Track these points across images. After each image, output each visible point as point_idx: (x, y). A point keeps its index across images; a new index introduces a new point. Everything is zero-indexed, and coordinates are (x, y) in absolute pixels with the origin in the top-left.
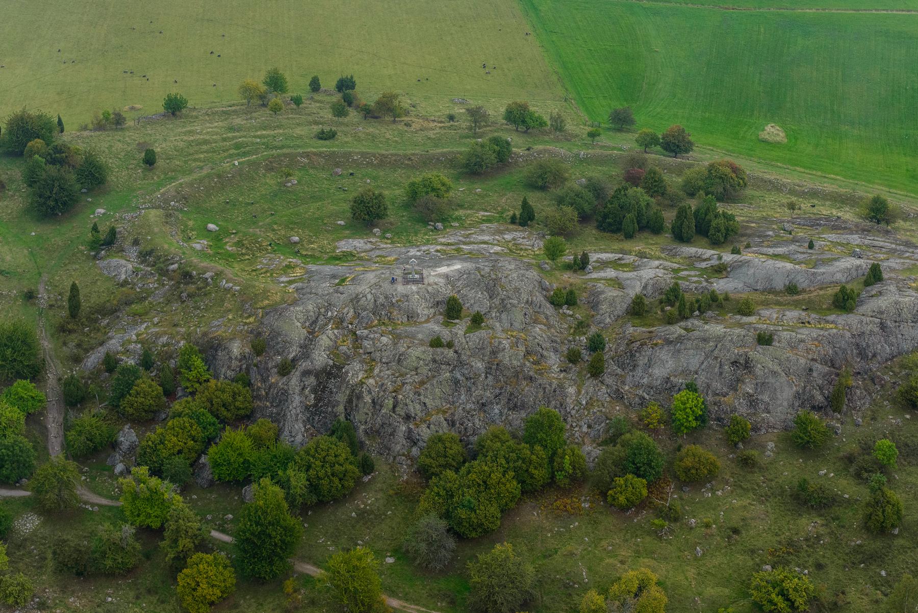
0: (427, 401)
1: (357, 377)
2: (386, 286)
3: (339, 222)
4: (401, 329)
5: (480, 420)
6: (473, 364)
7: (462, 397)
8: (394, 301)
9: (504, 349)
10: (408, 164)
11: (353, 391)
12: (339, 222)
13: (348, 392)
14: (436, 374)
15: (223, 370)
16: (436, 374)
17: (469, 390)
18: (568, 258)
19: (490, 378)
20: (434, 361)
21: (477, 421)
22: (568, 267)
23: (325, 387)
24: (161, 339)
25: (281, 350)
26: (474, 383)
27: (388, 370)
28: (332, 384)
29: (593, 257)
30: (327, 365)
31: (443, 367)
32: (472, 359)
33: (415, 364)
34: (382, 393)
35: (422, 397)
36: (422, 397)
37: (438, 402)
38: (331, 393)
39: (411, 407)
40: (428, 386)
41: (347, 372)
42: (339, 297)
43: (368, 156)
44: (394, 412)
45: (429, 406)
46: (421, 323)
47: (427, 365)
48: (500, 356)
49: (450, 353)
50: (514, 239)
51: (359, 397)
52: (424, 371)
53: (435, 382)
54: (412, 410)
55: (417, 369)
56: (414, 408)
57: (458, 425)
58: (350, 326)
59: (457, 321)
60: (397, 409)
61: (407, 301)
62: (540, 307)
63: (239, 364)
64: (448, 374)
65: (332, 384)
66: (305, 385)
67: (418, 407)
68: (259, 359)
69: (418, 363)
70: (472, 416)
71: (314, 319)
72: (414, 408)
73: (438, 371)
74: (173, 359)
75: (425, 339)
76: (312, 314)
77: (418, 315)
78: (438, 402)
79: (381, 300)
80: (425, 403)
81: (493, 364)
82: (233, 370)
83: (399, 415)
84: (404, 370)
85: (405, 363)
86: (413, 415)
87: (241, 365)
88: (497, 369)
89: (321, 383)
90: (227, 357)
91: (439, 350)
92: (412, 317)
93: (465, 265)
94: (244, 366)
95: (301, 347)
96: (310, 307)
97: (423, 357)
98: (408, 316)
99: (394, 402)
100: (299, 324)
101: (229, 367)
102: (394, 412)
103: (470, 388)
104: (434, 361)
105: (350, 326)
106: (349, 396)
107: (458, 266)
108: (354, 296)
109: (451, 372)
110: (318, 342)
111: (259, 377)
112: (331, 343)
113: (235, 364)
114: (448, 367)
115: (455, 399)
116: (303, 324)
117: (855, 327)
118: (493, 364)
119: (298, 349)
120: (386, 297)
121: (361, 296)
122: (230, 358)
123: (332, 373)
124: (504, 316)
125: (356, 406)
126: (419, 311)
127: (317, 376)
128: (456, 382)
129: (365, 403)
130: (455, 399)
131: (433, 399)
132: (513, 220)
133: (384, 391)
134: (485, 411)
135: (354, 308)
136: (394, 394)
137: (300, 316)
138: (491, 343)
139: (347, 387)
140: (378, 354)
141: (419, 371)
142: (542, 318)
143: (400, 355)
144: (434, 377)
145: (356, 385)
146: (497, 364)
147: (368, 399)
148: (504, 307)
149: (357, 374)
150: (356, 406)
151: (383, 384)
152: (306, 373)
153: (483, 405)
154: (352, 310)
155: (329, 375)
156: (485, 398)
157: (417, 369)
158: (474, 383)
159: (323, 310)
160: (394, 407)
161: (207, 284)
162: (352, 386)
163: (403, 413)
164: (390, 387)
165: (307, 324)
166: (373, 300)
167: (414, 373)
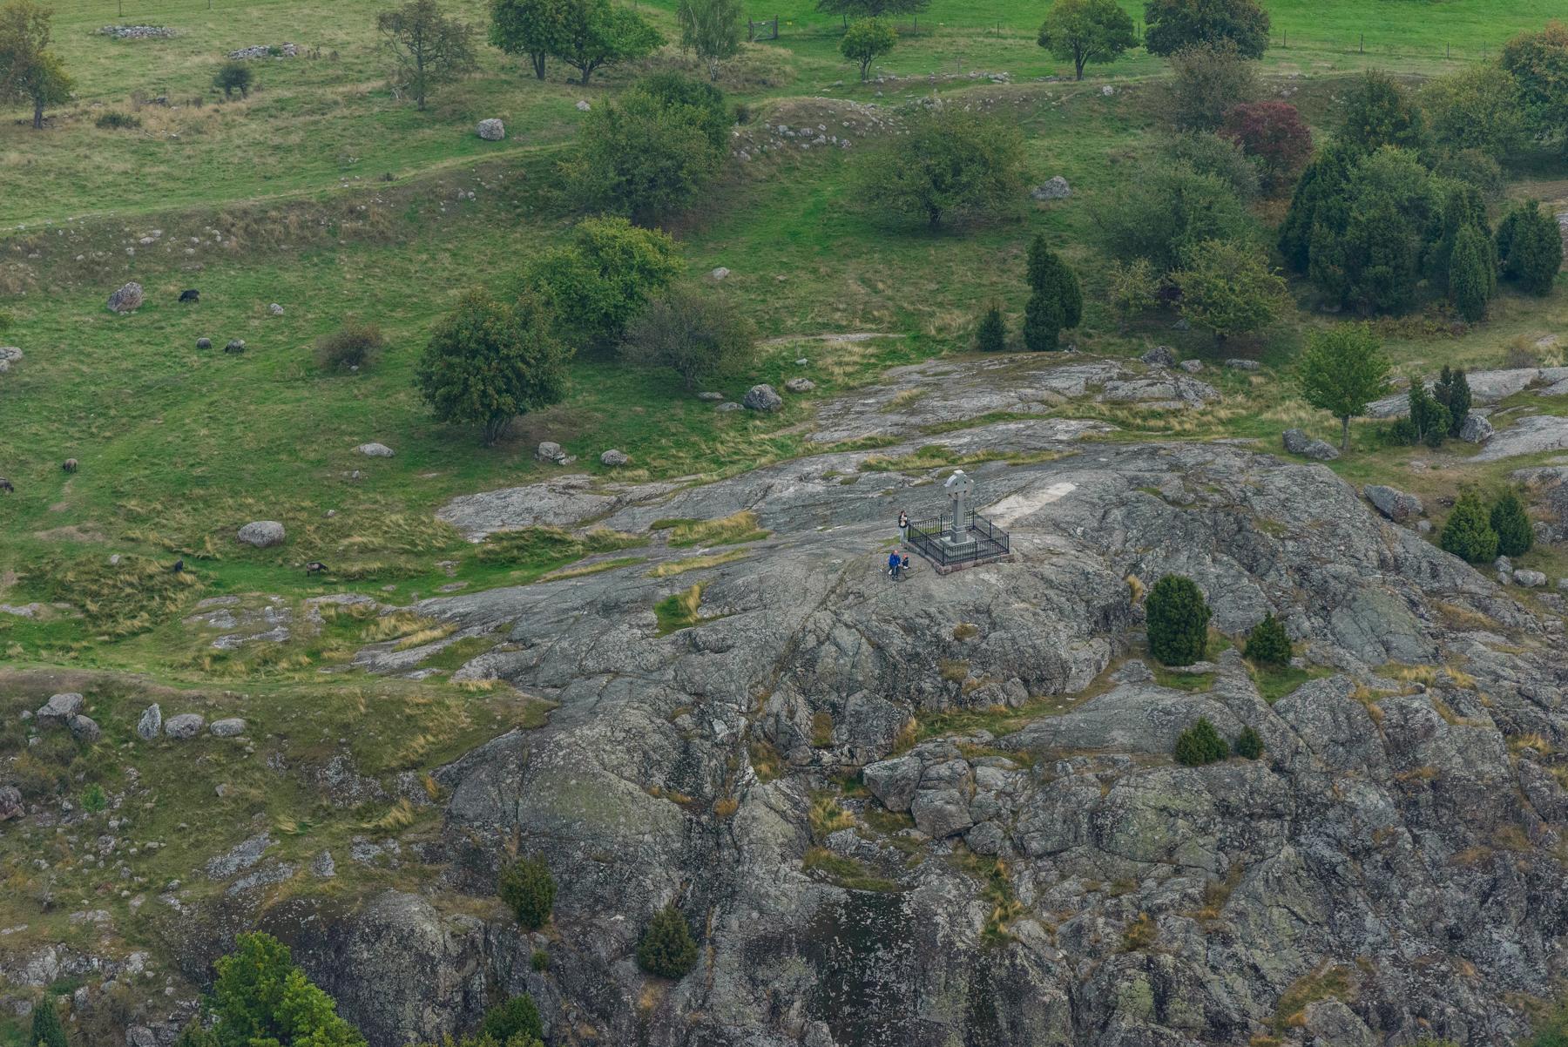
0: (1258, 957)
1: (970, 924)
2: (880, 590)
3: (369, 448)
4: (1029, 730)
5: (1472, 989)
6: (1352, 798)
7: (1370, 921)
8: (946, 634)
9: (1429, 730)
10: (356, 233)
11: (983, 973)
12: (369, 448)
13: (963, 984)
14: (1247, 857)
15: (408, 1012)
16: (1247, 857)
17: (1378, 894)
18: (1392, 407)
19: (1430, 839)
20: (1225, 810)
21: (1464, 993)
22: (1399, 436)
23: (859, 986)
24: (35, 966)
25: (607, 892)
26: (1387, 866)
27: (1063, 877)
28: (882, 966)
29: (1481, 383)
30: (827, 907)
31: (1263, 825)
32: (1341, 783)
33: (1161, 836)
34: (1087, 964)
35: (1238, 948)
36: (1238, 948)
37: (1293, 957)
38: (895, 999)
39: (1217, 990)
40: (1239, 902)
41: (925, 915)
42: (720, 666)
43: (193, 223)
44: (1162, 1019)
45: (1275, 977)
46: (1080, 695)
47: (1204, 831)
48: (1425, 751)
49: (1258, 772)
50: (1093, 388)
51: (1017, 991)
52: (1201, 852)
53: (1260, 886)
54: (1227, 1000)
55: (1171, 851)
56: (1231, 992)
57: (1409, 1021)
58: (827, 757)
59: (1202, 666)
60: (1175, 1005)
61: (994, 626)
62: (1435, 575)
63: (458, 977)
64: (1288, 851)
65: (882, 966)
66: (776, 994)
67: (1240, 985)
68: (541, 938)
69: (1172, 828)
70: (1442, 978)
71: (675, 755)
72: (1231, 992)
73: (1250, 842)
74: (142, 1021)
75: (1147, 742)
76: (656, 739)
77: (1064, 669)
78: (1293, 957)
79: (898, 641)
80: (1255, 968)
81: (1418, 789)
82: (443, 1005)
83: (1184, 1027)
84: (1125, 865)
85: (1122, 838)
86: (1236, 1017)
87: (466, 981)
88: (1436, 805)
89: (834, 973)
90: (407, 958)
91: (1222, 770)
92: (1041, 680)
93: (1084, 476)
94: (479, 982)
95: (683, 865)
96: (636, 718)
97: (1178, 804)
98: (1026, 682)
99: (1154, 987)
100: (624, 785)
101: (429, 995)
102: (1162, 1019)
103: (1377, 884)
104: (1225, 810)
105: (827, 757)
106: (972, 994)
107: (1061, 488)
108: (782, 647)
109: (1293, 838)
110: (746, 831)
111: (573, 1007)
112: (790, 829)
113: (447, 975)
114: (1276, 825)
115: (1346, 934)
116: (644, 780)
117: (1080, 888)
118: (1418, 789)
119: (676, 875)
120: (910, 629)
121: (811, 641)
122: (423, 959)
123: (867, 931)
124: (1341, 621)
125: (1014, 1026)
126: (1064, 655)
127: (809, 949)
128: (1325, 873)
129: (1047, 1008)
130: (1346, 934)
131: (1276, 948)
132: (991, 338)
133: (1094, 953)
134: (1470, 958)
135: (804, 692)
136: (1139, 955)
137: (618, 756)
138: (1373, 716)
139: (952, 966)
140: (995, 830)
141: (1182, 858)
142: (1462, 608)
143: (1093, 814)
144: (1244, 869)
145: (985, 951)
146: (1434, 785)
147: (1050, 991)
148: (1322, 590)
149: (962, 913)
150: (1014, 1026)
151: (1078, 931)
152: (762, 950)
153: (1454, 935)
154: (801, 699)
155: (858, 938)
156: (1450, 911)
157: (1171, 851)
158: (1387, 866)
159: (685, 720)
160: (1161, 1000)
161: (81, 739)
162: (973, 957)
163: (1197, 1018)
164: (1107, 931)
165: (659, 779)
166: (866, 648)
167: (1164, 869)
